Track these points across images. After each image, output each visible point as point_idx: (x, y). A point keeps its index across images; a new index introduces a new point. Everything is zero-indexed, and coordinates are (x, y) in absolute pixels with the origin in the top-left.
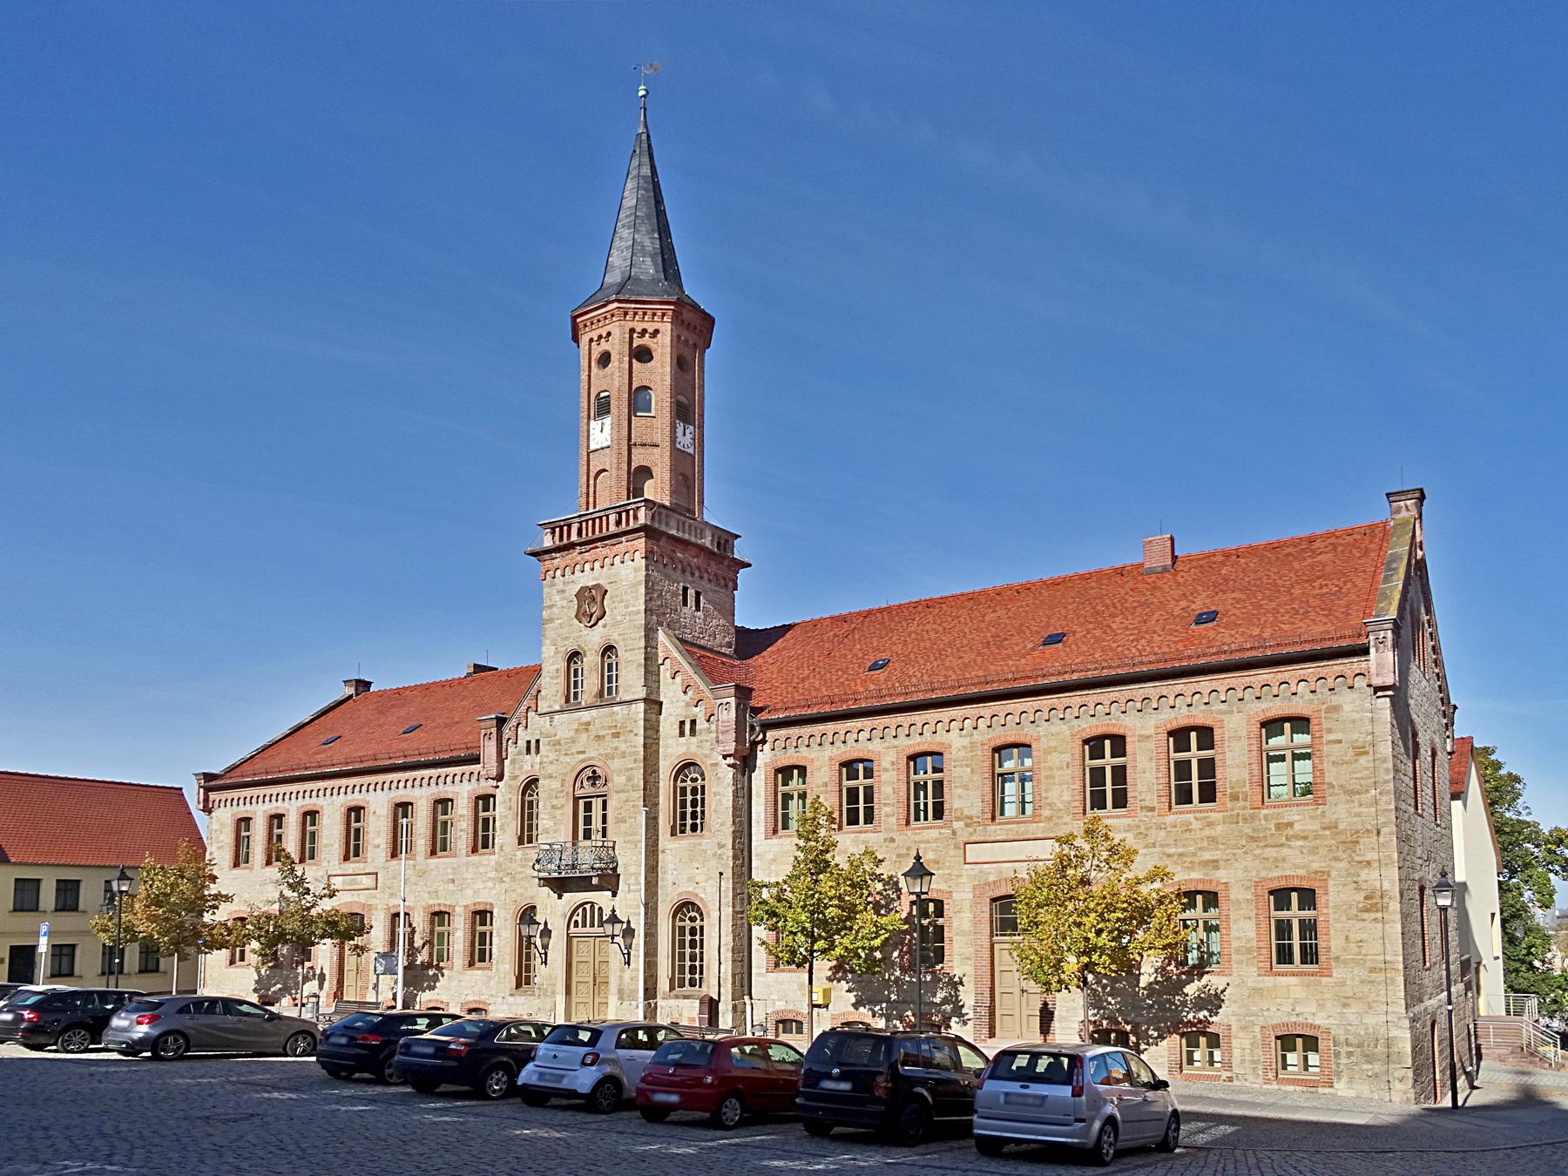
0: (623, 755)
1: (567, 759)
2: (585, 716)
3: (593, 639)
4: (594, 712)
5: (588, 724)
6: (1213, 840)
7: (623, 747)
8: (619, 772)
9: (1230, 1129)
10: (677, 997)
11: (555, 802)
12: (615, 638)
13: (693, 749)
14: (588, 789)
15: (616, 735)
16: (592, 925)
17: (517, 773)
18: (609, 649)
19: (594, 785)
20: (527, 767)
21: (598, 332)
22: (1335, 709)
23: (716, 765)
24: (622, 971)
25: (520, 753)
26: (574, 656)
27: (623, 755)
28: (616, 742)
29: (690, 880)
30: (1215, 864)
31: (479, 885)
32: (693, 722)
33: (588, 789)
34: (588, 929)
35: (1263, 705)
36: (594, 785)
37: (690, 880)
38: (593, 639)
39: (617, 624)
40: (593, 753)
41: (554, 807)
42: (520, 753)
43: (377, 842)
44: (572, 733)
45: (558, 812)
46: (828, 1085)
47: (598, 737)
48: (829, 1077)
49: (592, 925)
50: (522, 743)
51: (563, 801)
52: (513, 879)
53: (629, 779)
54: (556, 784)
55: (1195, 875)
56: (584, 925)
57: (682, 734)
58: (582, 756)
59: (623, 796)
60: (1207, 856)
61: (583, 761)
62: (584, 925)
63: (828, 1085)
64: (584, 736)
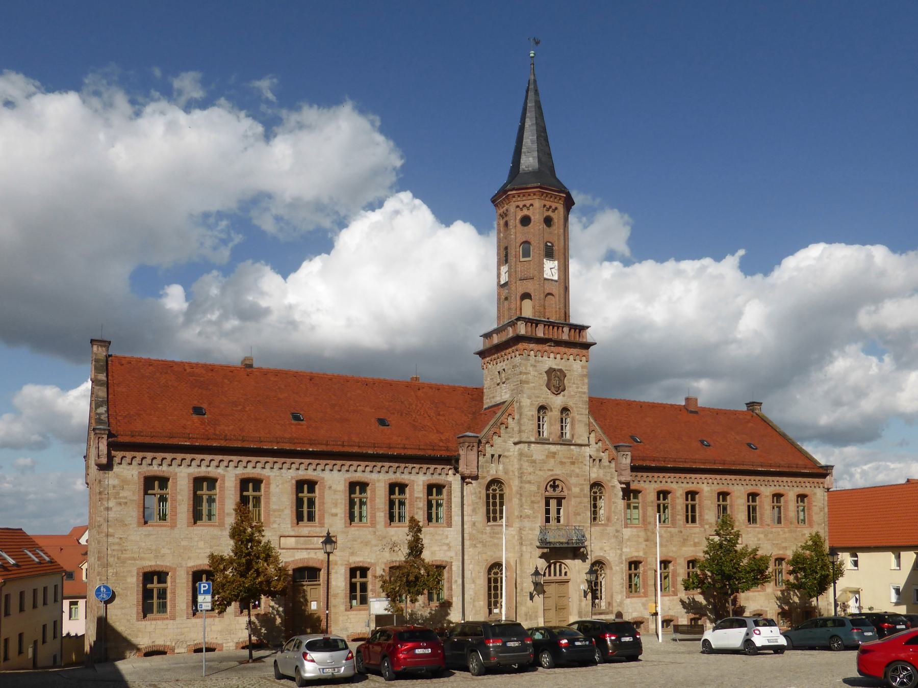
1: (541, 473)
3: (557, 401)
4: (559, 447)
5: (555, 453)
6: (785, 539)
7: (577, 471)
8: (575, 486)
11: (533, 499)
12: (571, 404)
13: (601, 475)
14: (551, 492)
15: (573, 463)
16: (555, 575)
18: (565, 410)
19: (554, 490)
20: (493, 472)
22: (815, 494)
23: (614, 487)
24: (580, 601)
25: (487, 462)
26: (542, 408)
27: (578, 476)
28: (572, 467)
29: (601, 549)
31: (436, 548)
33: (551, 492)
35: (688, 486)
36: (554, 490)
37: (601, 549)
38: (557, 401)
39: (571, 396)
40: (558, 472)
41: (532, 502)
42: (487, 462)
43: (334, 511)
44: (544, 457)
45: (536, 506)
46: (577, 643)
47: (562, 463)
48: (578, 640)
49: (555, 575)
50: (488, 456)
51: (539, 499)
52: (484, 545)
53: (582, 490)
54: (534, 488)
55: (781, 552)
58: (551, 473)
59: (578, 500)
60: (784, 545)
61: (552, 475)
62: (550, 575)
63: (577, 643)
64: (552, 461)
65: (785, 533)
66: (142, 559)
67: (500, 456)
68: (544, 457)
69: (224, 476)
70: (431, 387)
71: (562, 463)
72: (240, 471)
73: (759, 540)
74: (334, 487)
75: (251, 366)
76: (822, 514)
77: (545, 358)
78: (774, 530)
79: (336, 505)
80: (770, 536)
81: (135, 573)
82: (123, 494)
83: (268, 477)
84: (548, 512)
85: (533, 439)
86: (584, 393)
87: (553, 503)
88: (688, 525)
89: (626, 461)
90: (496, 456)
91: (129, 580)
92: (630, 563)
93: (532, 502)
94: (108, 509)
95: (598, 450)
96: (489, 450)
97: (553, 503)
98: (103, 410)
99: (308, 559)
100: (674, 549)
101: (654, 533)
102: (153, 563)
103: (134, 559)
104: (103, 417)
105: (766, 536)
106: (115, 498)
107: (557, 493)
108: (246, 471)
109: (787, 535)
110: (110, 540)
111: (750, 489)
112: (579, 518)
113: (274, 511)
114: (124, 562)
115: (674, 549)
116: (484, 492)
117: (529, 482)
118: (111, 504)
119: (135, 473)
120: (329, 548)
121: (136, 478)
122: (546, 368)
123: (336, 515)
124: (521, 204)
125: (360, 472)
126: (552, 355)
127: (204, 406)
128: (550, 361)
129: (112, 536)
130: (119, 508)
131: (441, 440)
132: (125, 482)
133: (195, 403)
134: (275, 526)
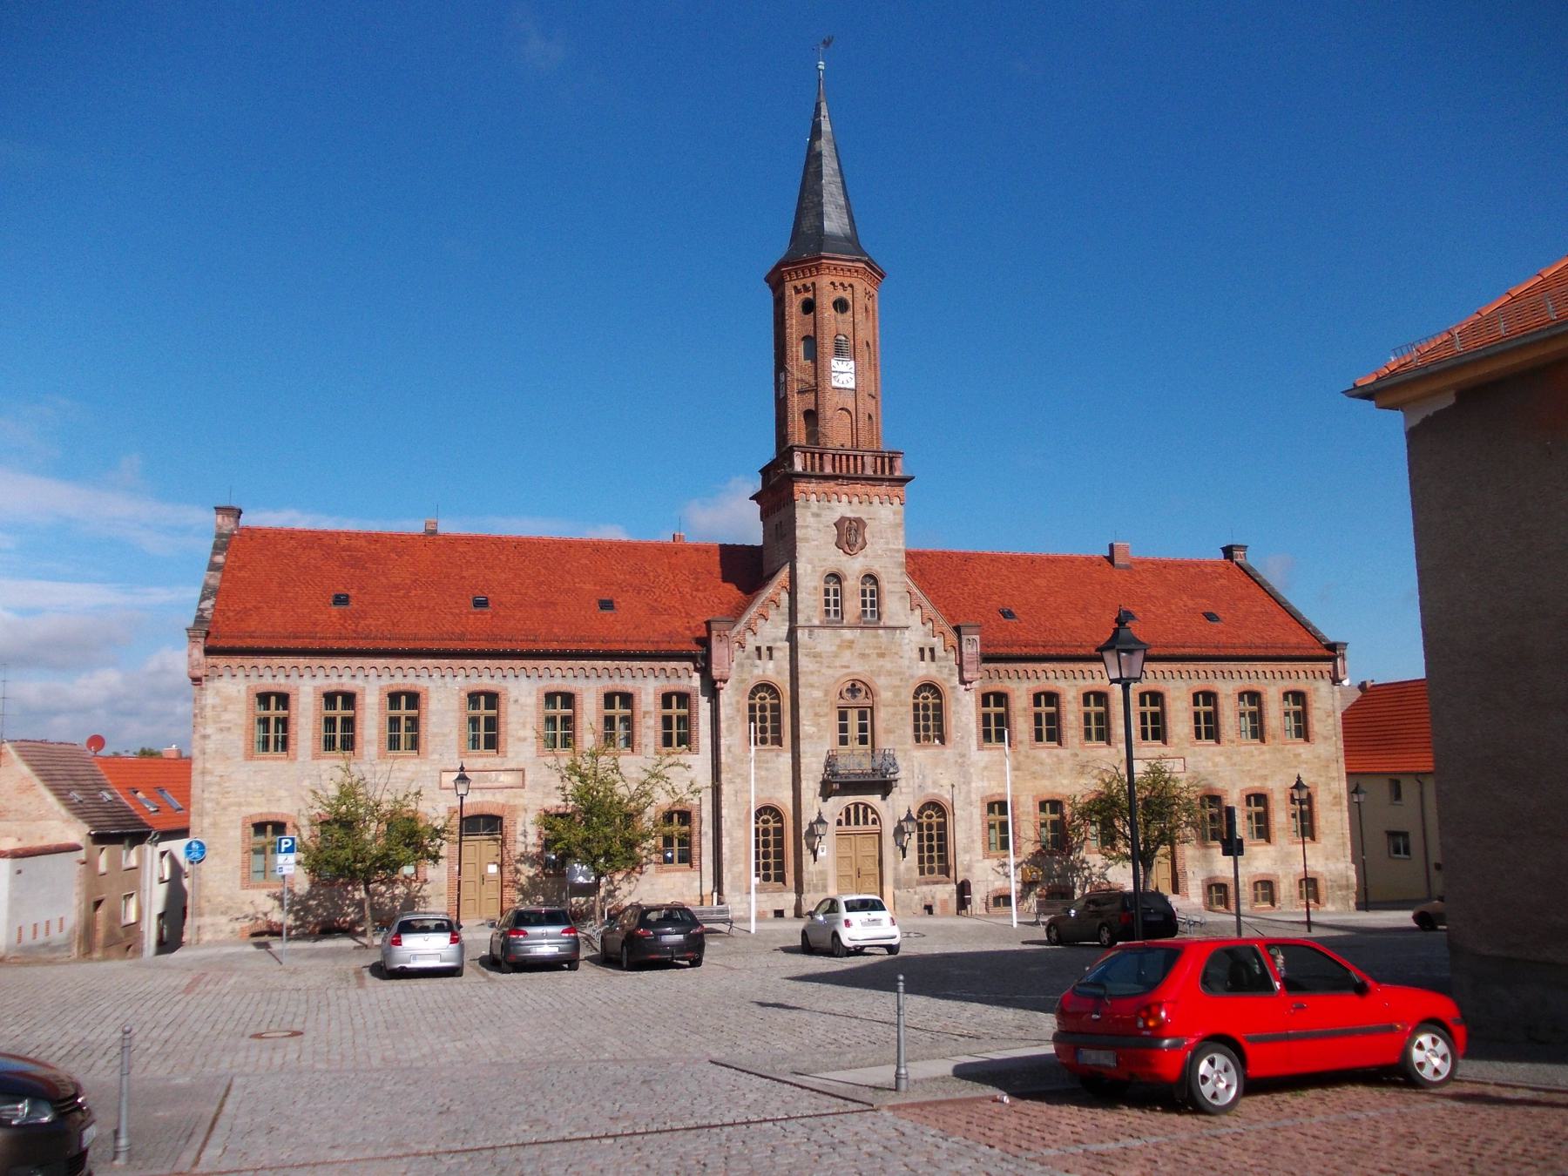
0: (889, 673)
1: (830, 672)
2: (848, 634)
5: (852, 642)
6: (1264, 762)
7: (889, 666)
9: (1341, 933)
10: (927, 883)
12: (876, 568)
14: (848, 700)
15: (882, 655)
16: (857, 823)
17: (745, 676)
19: (854, 697)
20: (758, 672)
21: (842, 279)
22: (1317, 689)
24: (897, 862)
27: (889, 673)
28: (881, 662)
30: (1265, 778)
32: (932, 650)
33: (848, 700)
34: (853, 827)
36: (854, 697)
38: (854, 567)
40: (859, 669)
41: (816, 714)
43: (522, 733)
44: (834, 648)
45: (822, 720)
49: (857, 823)
53: (897, 695)
54: (818, 694)
55: (1257, 784)
56: (848, 823)
57: (922, 659)
59: (890, 710)
62: (848, 823)
64: (848, 653)
65: (1263, 753)
66: (249, 804)
67: (770, 649)
68: (834, 648)
69: (364, 689)
70: (697, 549)
71: (863, 656)
72: (386, 681)
73: (1216, 765)
74: (522, 700)
75: (434, 533)
76: (1331, 721)
77: (834, 503)
78: (1243, 749)
79: (524, 725)
80: (1236, 758)
81: (240, 823)
82: (226, 716)
83: (427, 689)
84: (843, 728)
85: (816, 622)
86: (898, 551)
87: (853, 716)
88: (1089, 744)
89: (972, 649)
90: (764, 649)
91: (232, 833)
92: (991, 807)
93: (816, 714)
94: (205, 737)
95: (926, 635)
96: (751, 642)
97: (853, 716)
98: (208, 604)
99: (482, 804)
100: (1065, 782)
101: (747, 780)
102: (264, 810)
103: (240, 805)
104: (206, 614)
105: (1229, 758)
106: (215, 722)
107: (861, 700)
108: (393, 682)
109: (1267, 756)
110: (208, 778)
111: (1199, 685)
112: (892, 737)
113: (435, 735)
114: (225, 809)
115: (1065, 782)
116: (746, 702)
117: (812, 686)
118: (209, 731)
119: (243, 688)
120: (462, 789)
121: (243, 694)
122: (837, 517)
123: (525, 739)
124: (837, 280)
125: (560, 676)
126: (844, 498)
127: (352, 593)
128: (843, 508)
129: (211, 773)
130: (219, 737)
131: (689, 628)
132: (228, 700)
133: (341, 589)
134: (436, 756)
